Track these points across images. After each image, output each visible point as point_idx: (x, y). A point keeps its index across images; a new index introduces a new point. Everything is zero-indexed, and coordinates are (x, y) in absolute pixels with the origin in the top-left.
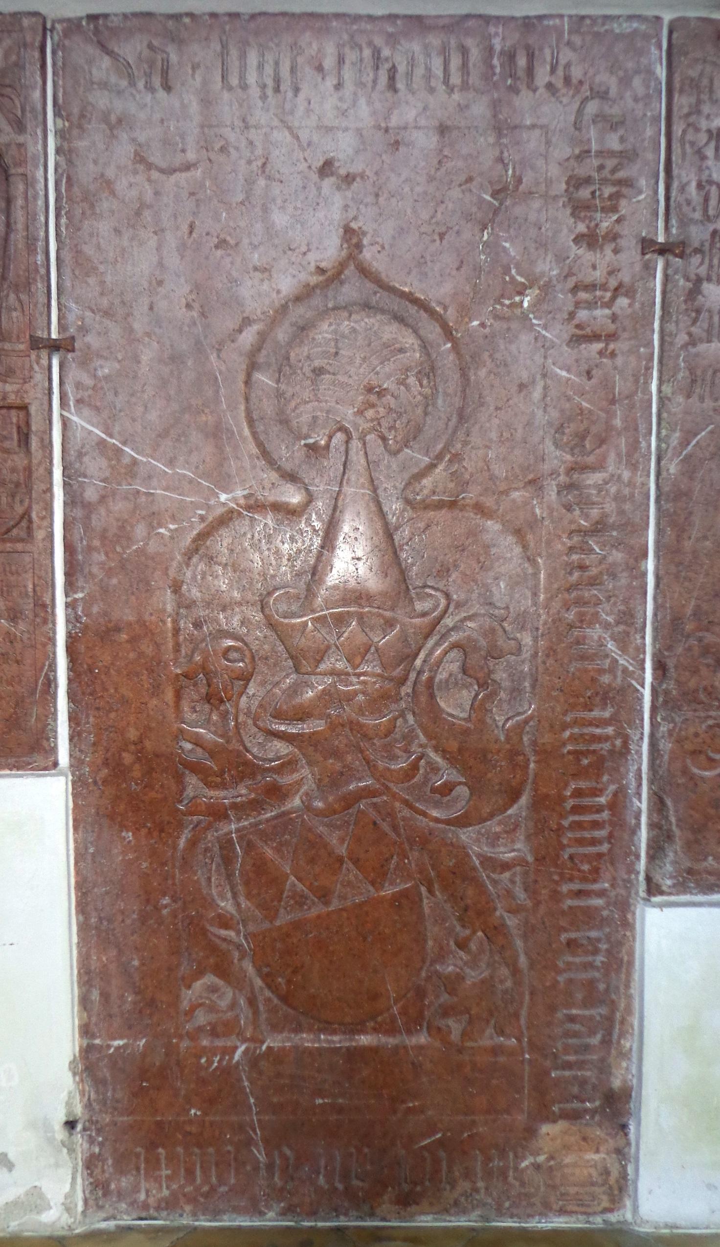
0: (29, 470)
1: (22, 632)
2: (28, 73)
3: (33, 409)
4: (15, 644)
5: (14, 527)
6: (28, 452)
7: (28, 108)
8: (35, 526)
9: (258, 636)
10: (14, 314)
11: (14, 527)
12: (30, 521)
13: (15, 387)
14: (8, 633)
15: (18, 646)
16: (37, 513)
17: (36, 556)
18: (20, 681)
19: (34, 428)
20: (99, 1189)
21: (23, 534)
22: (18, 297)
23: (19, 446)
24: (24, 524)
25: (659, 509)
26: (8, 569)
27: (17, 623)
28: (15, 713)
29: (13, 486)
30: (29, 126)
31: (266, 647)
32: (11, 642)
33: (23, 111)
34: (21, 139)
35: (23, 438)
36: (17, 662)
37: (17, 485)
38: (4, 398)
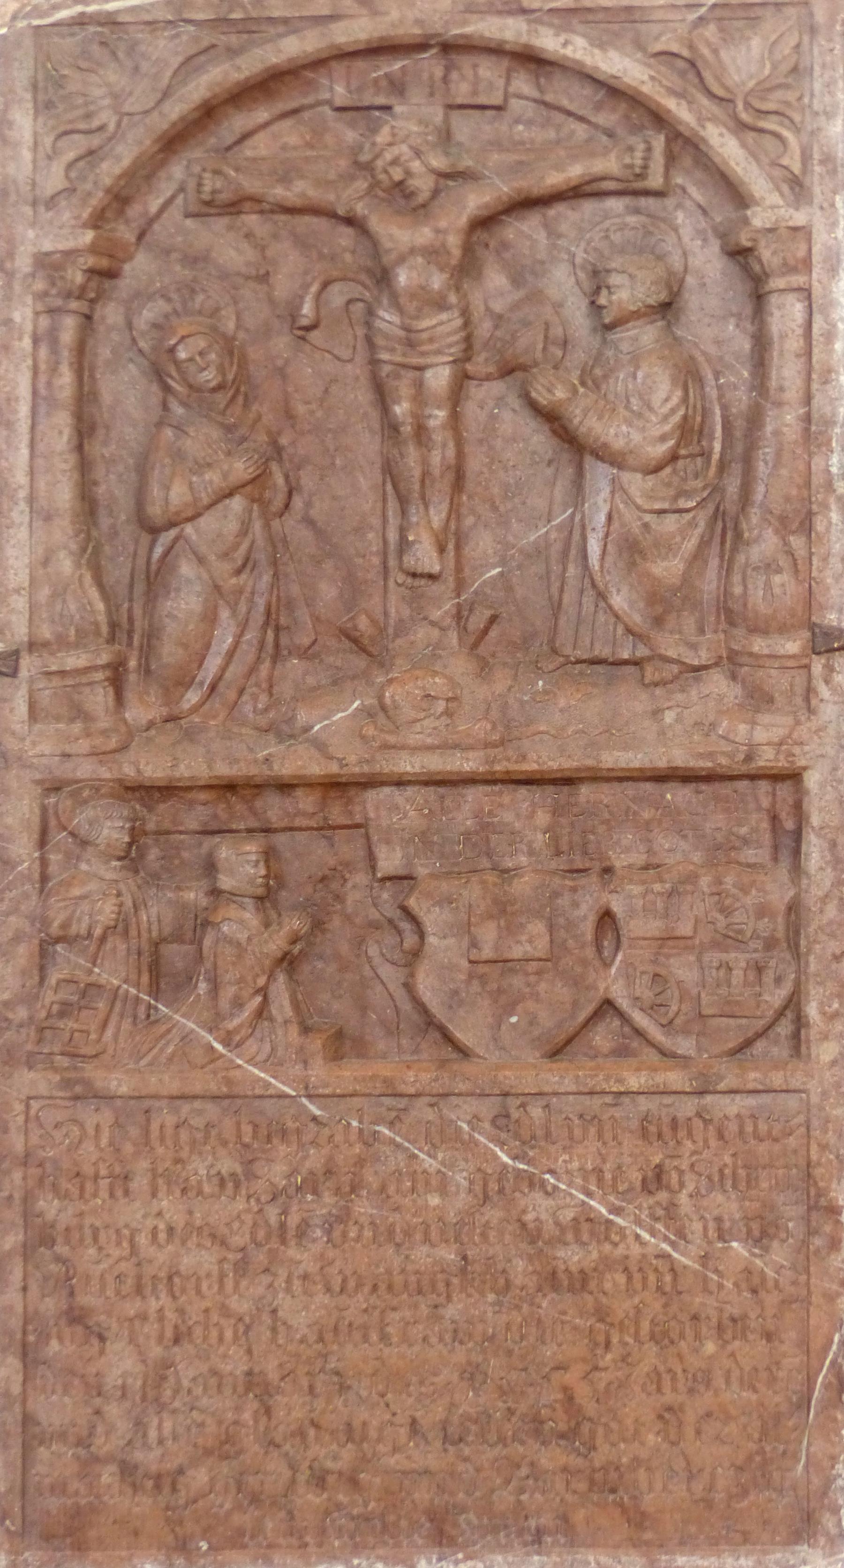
0: (794, 908)
1: (779, 1269)
2: (817, 86)
3: (812, 780)
4: (763, 1294)
5: (759, 1035)
6: (797, 869)
7: (816, 156)
8: (813, 1033)
9: (94, 1005)
10: (777, 579)
11: (759, 1035)
12: (800, 1022)
13: (776, 734)
14: (748, 1271)
15: (771, 1300)
16: (821, 1004)
17: (815, 1099)
18: (773, 1380)
19: (815, 820)
20: (121, 268)
21: (781, 1051)
22: (786, 543)
23: (775, 859)
24: (784, 1028)
25: (260, 1079)
26: (749, 1129)
27: (766, 1249)
28: (761, 1452)
29: (758, 944)
30: (817, 190)
31: (536, 1112)
32: (754, 1291)
33: (806, 158)
34: (799, 218)
35: (788, 841)
36: (769, 1336)
37: (770, 944)
38: (749, 758)
